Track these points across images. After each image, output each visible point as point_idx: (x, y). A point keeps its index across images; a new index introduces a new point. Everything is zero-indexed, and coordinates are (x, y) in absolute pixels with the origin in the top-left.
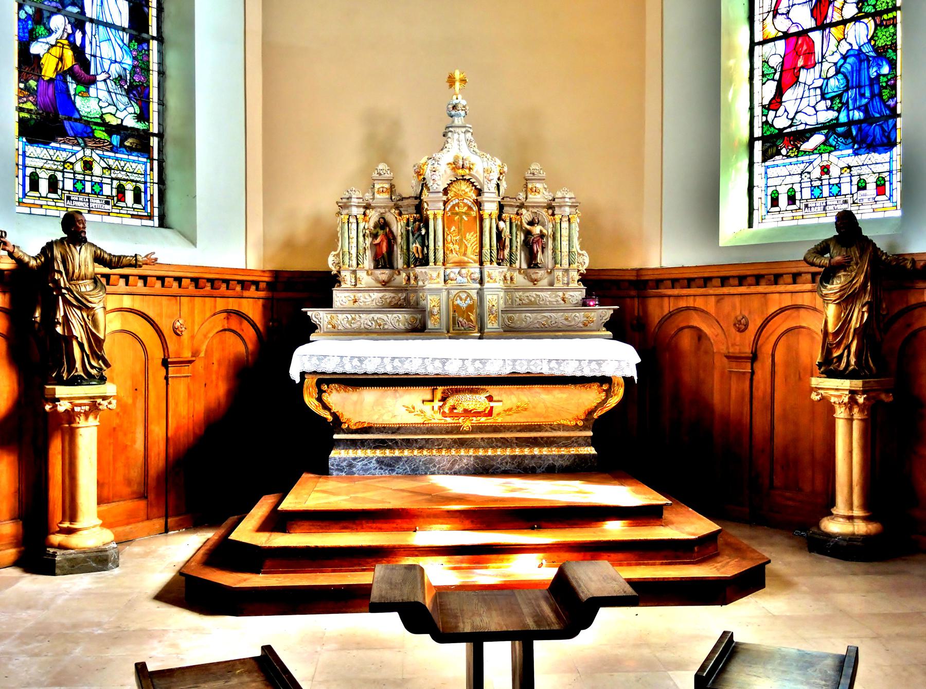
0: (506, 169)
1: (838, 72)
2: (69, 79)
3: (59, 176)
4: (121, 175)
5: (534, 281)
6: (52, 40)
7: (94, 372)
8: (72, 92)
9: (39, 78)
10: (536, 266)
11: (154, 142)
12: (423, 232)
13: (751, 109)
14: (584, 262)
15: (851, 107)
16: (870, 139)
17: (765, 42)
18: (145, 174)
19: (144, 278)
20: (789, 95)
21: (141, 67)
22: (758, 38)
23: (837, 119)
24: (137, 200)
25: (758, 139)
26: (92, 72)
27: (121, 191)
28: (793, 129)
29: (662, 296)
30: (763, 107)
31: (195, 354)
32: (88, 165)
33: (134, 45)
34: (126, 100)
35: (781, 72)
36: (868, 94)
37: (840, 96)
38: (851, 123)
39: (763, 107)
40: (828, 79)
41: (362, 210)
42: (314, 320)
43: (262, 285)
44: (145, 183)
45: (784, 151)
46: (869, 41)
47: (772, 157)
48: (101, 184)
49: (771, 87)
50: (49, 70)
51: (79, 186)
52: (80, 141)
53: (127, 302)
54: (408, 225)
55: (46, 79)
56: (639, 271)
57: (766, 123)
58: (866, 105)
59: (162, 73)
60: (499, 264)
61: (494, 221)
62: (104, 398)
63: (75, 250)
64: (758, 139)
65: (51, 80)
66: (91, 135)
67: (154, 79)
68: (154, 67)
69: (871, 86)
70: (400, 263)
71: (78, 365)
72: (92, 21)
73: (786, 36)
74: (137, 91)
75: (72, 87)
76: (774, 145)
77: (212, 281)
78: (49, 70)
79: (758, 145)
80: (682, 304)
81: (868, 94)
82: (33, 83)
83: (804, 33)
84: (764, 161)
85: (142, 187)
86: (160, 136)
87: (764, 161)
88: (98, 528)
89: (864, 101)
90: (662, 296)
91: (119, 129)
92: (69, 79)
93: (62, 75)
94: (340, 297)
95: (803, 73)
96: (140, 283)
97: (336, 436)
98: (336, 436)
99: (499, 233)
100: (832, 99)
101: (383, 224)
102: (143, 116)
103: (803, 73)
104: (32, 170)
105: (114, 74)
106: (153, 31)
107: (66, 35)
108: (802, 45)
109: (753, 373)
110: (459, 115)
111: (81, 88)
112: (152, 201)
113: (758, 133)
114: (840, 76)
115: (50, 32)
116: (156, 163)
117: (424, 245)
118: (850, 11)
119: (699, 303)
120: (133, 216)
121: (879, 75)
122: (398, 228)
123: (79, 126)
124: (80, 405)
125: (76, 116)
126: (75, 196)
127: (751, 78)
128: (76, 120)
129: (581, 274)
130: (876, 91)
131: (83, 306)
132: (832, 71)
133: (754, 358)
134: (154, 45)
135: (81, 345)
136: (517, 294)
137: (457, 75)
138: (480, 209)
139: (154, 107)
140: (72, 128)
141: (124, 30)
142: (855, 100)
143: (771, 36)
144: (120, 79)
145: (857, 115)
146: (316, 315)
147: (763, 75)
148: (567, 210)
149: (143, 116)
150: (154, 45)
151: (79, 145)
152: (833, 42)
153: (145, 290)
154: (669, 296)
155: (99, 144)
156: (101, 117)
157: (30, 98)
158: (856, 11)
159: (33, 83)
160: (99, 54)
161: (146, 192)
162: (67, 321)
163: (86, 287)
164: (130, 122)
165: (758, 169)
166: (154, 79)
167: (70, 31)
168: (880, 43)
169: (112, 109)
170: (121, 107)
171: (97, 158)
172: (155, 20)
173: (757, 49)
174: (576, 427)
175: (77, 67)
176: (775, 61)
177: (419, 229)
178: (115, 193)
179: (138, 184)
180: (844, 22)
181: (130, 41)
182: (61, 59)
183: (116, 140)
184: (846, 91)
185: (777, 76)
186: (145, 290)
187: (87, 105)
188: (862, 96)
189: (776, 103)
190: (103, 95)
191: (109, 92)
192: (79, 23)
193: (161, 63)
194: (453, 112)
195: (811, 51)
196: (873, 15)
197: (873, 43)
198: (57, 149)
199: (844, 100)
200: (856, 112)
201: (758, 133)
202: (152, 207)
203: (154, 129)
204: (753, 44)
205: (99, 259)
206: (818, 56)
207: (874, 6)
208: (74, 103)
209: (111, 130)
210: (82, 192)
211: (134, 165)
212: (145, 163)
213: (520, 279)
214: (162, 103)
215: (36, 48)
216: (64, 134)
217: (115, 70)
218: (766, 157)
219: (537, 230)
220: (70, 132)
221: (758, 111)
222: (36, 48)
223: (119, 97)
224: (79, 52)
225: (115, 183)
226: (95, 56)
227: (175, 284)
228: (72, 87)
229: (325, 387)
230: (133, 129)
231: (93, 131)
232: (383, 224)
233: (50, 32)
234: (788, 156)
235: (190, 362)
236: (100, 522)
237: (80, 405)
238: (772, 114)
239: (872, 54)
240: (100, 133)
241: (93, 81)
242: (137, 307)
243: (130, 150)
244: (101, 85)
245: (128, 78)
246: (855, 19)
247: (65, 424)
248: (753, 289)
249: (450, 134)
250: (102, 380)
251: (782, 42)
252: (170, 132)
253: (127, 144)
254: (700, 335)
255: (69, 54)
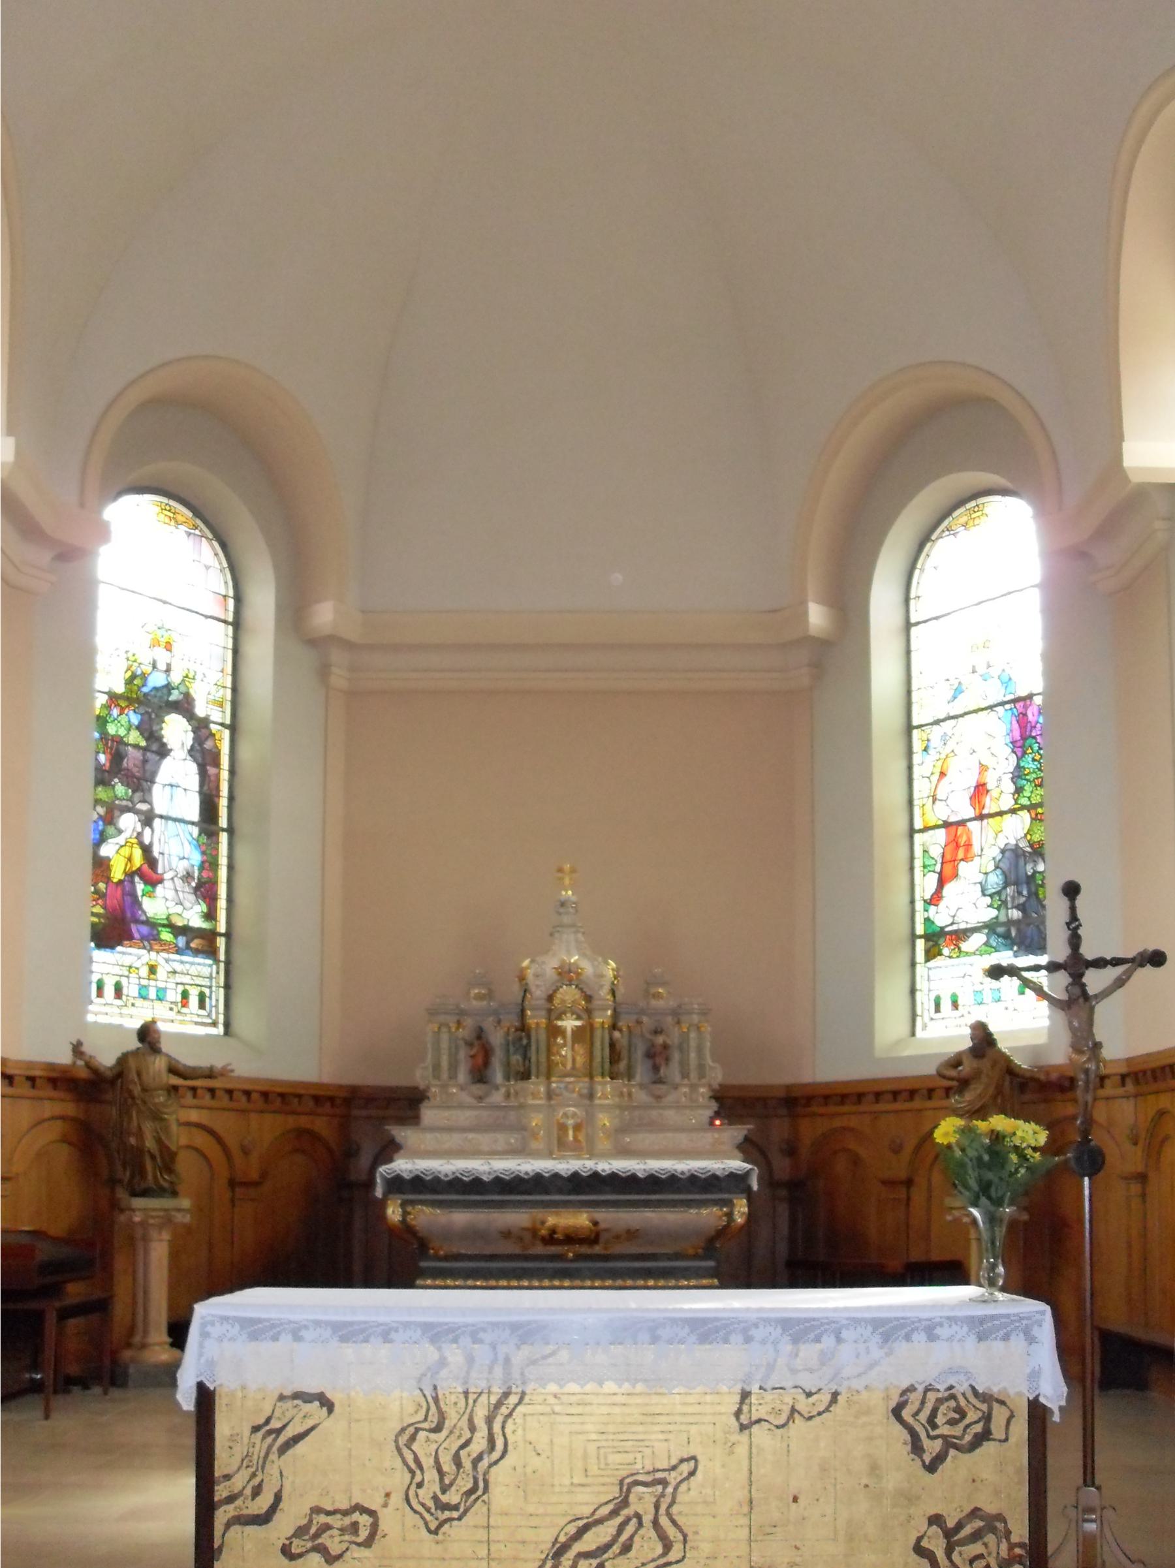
0: (621, 973)
1: (997, 867)
2: (137, 879)
3: (124, 981)
4: (187, 979)
5: (658, 1098)
6: (121, 839)
7: (165, 1185)
8: (139, 893)
9: (108, 880)
10: (660, 1081)
11: (221, 942)
12: (525, 1042)
13: (912, 902)
14: (717, 1076)
15: (1010, 906)
16: (1028, 940)
17: (926, 829)
18: (211, 978)
19: (212, 1091)
20: (948, 889)
21: (210, 864)
22: (918, 825)
23: (997, 917)
24: (202, 1005)
25: (920, 937)
26: (160, 871)
27: (185, 995)
28: (955, 927)
29: (813, 1115)
30: (925, 901)
31: (264, 1175)
32: (152, 970)
33: (204, 839)
34: (192, 897)
35: (942, 863)
36: (1025, 893)
37: (999, 893)
38: (1010, 922)
39: (925, 901)
40: (986, 874)
41: (455, 1018)
42: (398, 1139)
43: (338, 1102)
44: (210, 987)
45: (946, 951)
46: (1025, 836)
47: (934, 957)
48: (165, 989)
49: (932, 881)
50: (117, 874)
51: (144, 993)
52: (146, 943)
53: (194, 1116)
54: (508, 1033)
55: (115, 880)
56: (789, 1088)
57: (927, 920)
58: (1023, 904)
59: (231, 867)
60: (612, 1078)
61: (607, 1032)
62: (179, 1210)
63: (151, 1059)
64: (920, 937)
65: (121, 882)
66: (157, 938)
67: (223, 873)
68: (223, 861)
69: (1028, 883)
70: (499, 1077)
71: (150, 1177)
72: (161, 817)
73: (946, 825)
74: (205, 890)
75: (140, 887)
76: (936, 944)
77: (282, 1095)
78: (117, 874)
79: (920, 944)
80: (837, 1123)
81: (1025, 893)
82: (102, 886)
83: (962, 823)
84: (927, 960)
85: (207, 991)
86: (228, 935)
87: (927, 960)
88: (167, 1347)
89: (1022, 900)
90: (813, 1115)
91: (184, 931)
92: (137, 879)
93: (130, 875)
94: (429, 1114)
95: (962, 865)
96: (208, 1096)
97: (423, 1264)
98: (423, 1264)
99: (612, 1045)
100: (991, 896)
101: (480, 1034)
102: (210, 916)
103: (962, 865)
104: (99, 976)
105: (182, 873)
106: (223, 822)
107: (135, 834)
108: (961, 835)
109: (908, 1199)
110: (567, 913)
111: (149, 888)
112: (216, 1006)
113: (920, 930)
114: (998, 872)
115: (120, 832)
116: (222, 965)
117: (525, 1057)
118: (1007, 802)
119: (853, 1122)
120: (196, 1023)
121: (1035, 872)
122: (496, 1038)
123: (145, 930)
124: (153, 1217)
125: (143, 918)
126: (139, 1002)
127: (912, 869)
128: (143, 923)
129: (713, 1090)
130: (1033, 889)
131: (157, 1116)
132: (991, 866)
133: (909, 1183)
134: (224, 837)
135: (153, 1157)
136: (636, 1113)
137: (567, 867)
138: (590, 1017)
139: (222, 904)
140: (138, 931)
141: (193, 823)
142: (1013, 898)
143: (931, 824)
144: (188, 877)
145: (1015, 914)
146: (401, 1134)
147: (924, 867)
148: (695, 1018)
149: (210, 916)
150: (224, 837)
151: (144, 948)
152: (991, 834)
153: (213, 1103)
154: (822, 1115)
155: (165, 947)
156: (168, 919)
157: (100, 901)
158: (1013, 802)
159: (102, 886)
160: (166, 852)
161: (210, 998)
162: (140, 1134)
163: (161, 1098)
164: (197, 922)
165: (920, 970)
166: (223, 873)
167: (139, 830)
168: (1036, 838)
169: (179, 909)
170: (187, 904)
171: (162, 962)
172: (225, 810)
173: (917, 836)
174: (696, 1257)
175: (146, 867)
176: (936, 852)
177: (521, 1039)
178: (179, 999)
179: (204, 989)
180: (1001, 814)
181: (200, 835)
182: (130, 859)
183: (181, 941)
184: (1005, 888)
185: (938, 868)
186: (213, 1103)
187: (157, 905)
188: (1020, 893)
189: (936, 899)
190: (170, 894)
191: (176, 891)
192: (148, 819)
193: (230, 857)
194: (562, 910)
195: (968, 845)
196: (1029, 808)
197: (1029, 837)
198: (123, 953)
199: (1003, 898)
200: (1015, 911)
201: (920, 930)
202: (217, 1013)
203: (222, 928)
204: (912, 831)
205: (174, 1070)
206: (976, 849)
207: (1029, 798)
208: (140, 905)
209: (178, 931)
210: (145, 998)
211: (199, 968)
212: (210, 966)
213: (641, 1096)
214: (230, 900)
215: (106, 850)
216: (130, 937)
217: (182, 866)
218: (930, 955)
219: (660, 1040)
220: (136, 935)
221: (919, 905)
222: (106, 850)
223: (186, 895)
224: (147, 850)
225: (180, 988)
226: (162, 854)
227: (244, 1099)
228: (140, 887)
229: (409, 1209)
230: (200, 930)
231: (159, 933)
232: (480, 1034)
233: (120, 832)
234: (950, 957)
235: (256, 1184)
236: (169, 1340)
237: (153, 1217)
238: (932, 909)
239: (1029, 849)
240: (166, 935)
241: (161, 881)
242: (205, 1121)
243: (197, 952)
244: (168, 884)
245: (196, 875)
246: (1013, 811)
247: (135, 1240)
248: (907, 1105)
249: (557, 935)
250: (174, 1194)
251: (943, 831)
252: (239, 931)
253: (193, 945)
254: (856, 1161)
255: (138, 854)
